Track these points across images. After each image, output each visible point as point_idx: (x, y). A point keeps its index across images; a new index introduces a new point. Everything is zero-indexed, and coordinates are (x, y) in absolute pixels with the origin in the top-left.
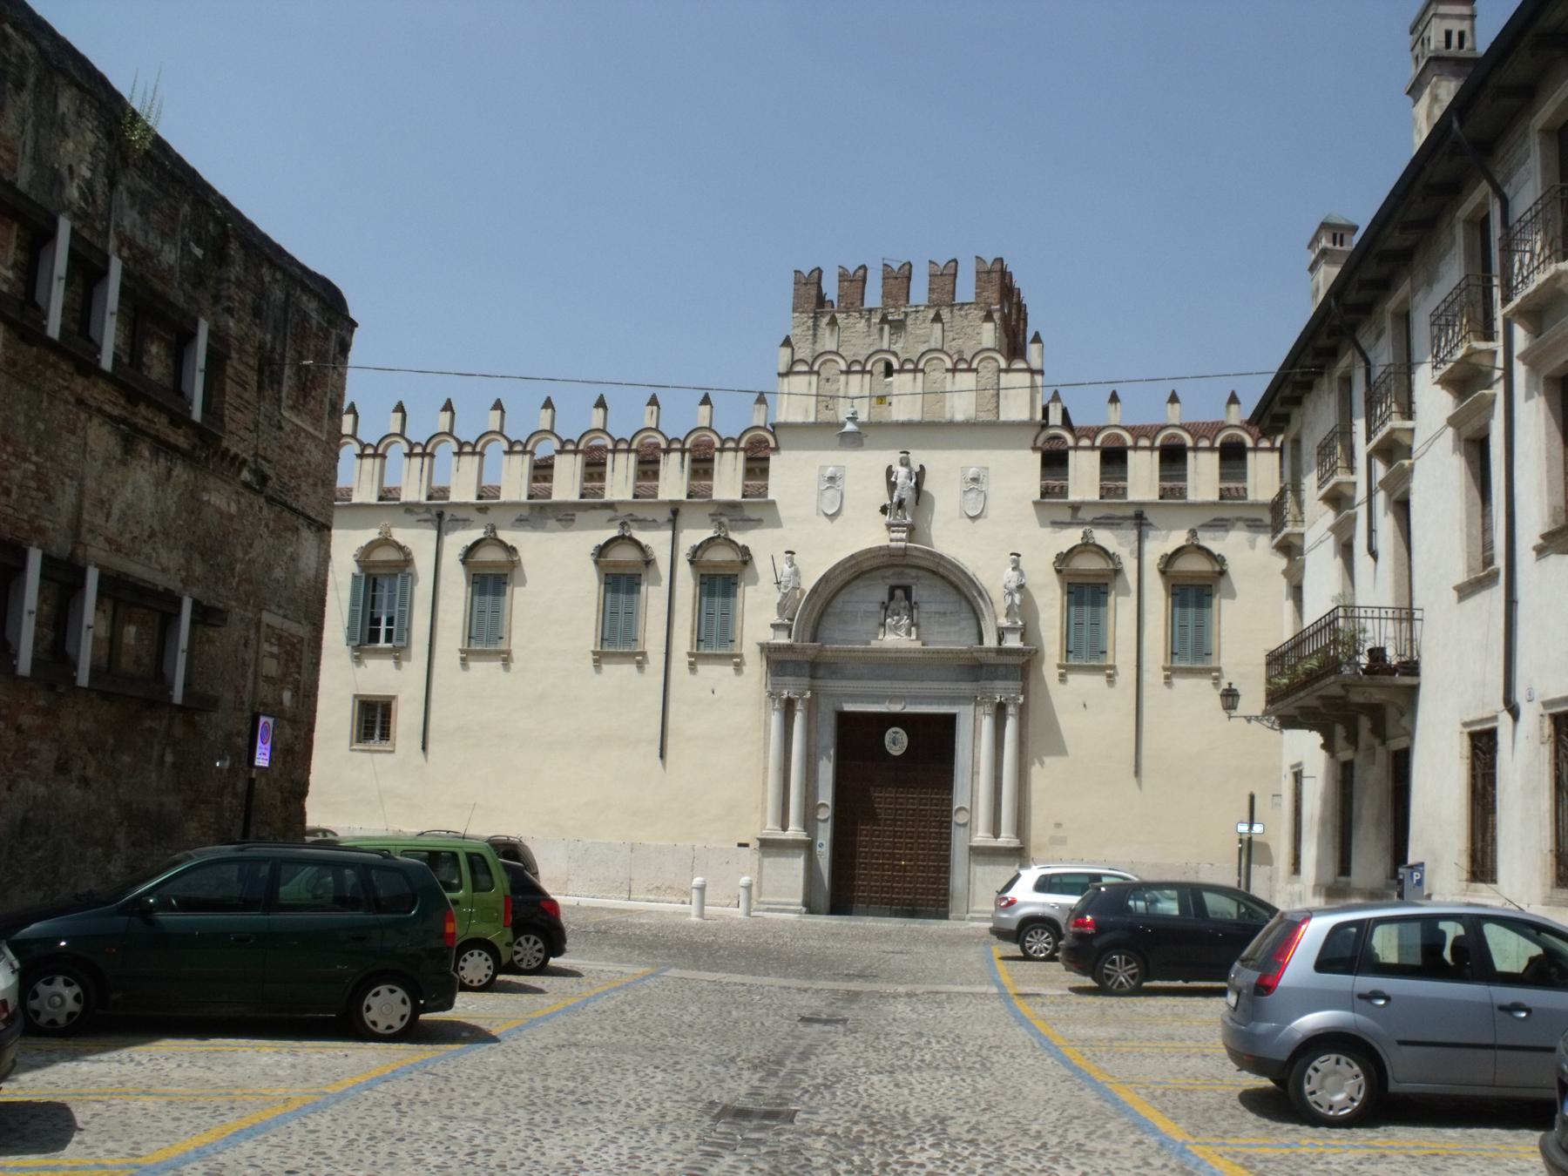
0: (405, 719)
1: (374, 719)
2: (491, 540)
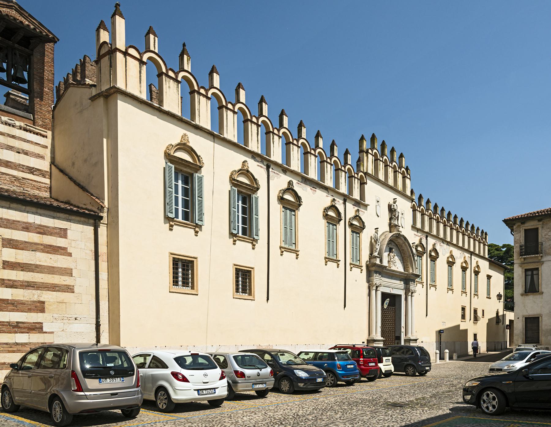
0: (258, 281)
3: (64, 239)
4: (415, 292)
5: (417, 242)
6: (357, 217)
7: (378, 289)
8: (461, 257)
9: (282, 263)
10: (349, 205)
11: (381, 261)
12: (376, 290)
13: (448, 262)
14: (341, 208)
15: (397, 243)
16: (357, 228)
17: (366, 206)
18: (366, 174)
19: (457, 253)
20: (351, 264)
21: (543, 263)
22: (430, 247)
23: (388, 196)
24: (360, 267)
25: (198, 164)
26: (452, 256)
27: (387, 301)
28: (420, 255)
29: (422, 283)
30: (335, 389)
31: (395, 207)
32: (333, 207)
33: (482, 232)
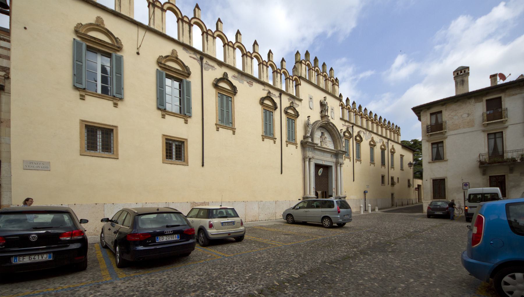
0: (193, 151)
1: (175, 150)
2: (224, 78)
3: (186, 167)
4: (343, 164)
5: (344, 129)
6: (291, 107)
7: (311, 160)
8: (380, 142)
9: (219, 138)
10: (285, 98)
11: (312, 140)
12: (309, 162)
13: (370, 144)
14: (277, 100)
15: (327, 127)
16: (292, 115)
17: (301, 100)
18: (300, 77)
19: (376, 138)
20: (286, 142)
21: (446, 138)
22: (355, 134)
23: (319, 96)
24: (296, 144)
25: (116, 45)
26: (373, 140)
27: (321, 170)
28: (348, 139)
29: (349, 158)
30: (331, 230)
31: (326, 103)
32: (268, 97)
33: (396, 126)
